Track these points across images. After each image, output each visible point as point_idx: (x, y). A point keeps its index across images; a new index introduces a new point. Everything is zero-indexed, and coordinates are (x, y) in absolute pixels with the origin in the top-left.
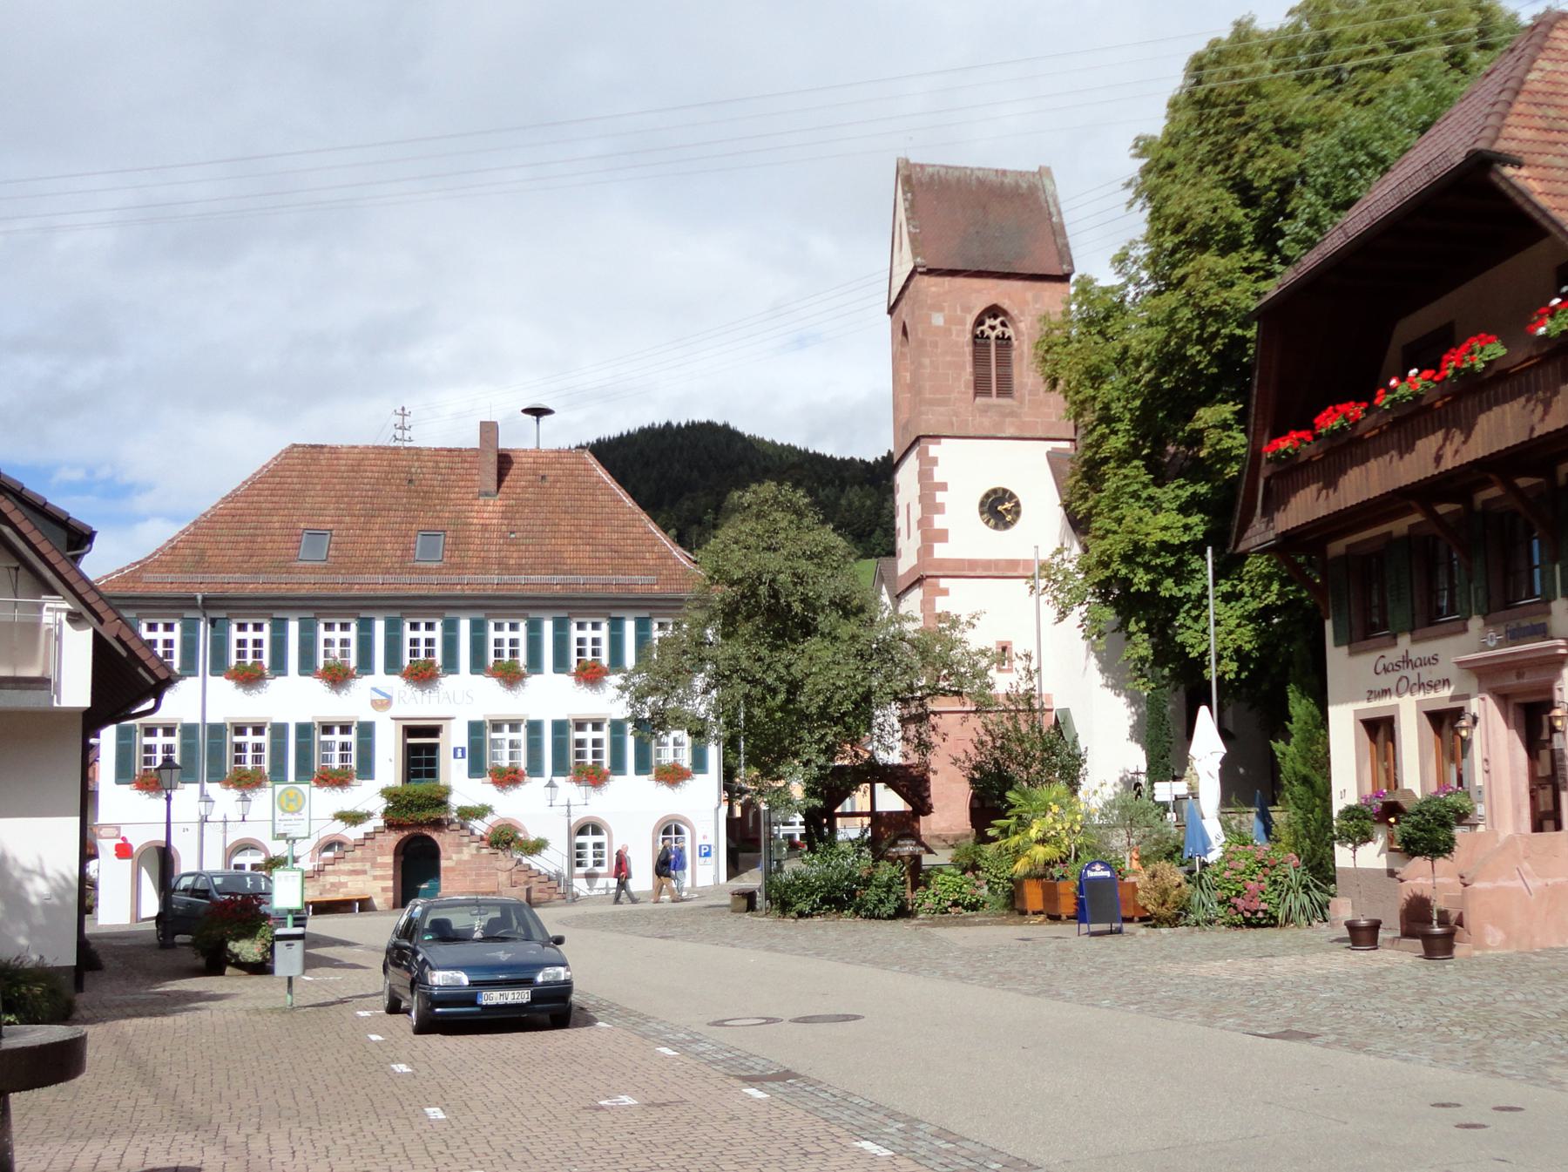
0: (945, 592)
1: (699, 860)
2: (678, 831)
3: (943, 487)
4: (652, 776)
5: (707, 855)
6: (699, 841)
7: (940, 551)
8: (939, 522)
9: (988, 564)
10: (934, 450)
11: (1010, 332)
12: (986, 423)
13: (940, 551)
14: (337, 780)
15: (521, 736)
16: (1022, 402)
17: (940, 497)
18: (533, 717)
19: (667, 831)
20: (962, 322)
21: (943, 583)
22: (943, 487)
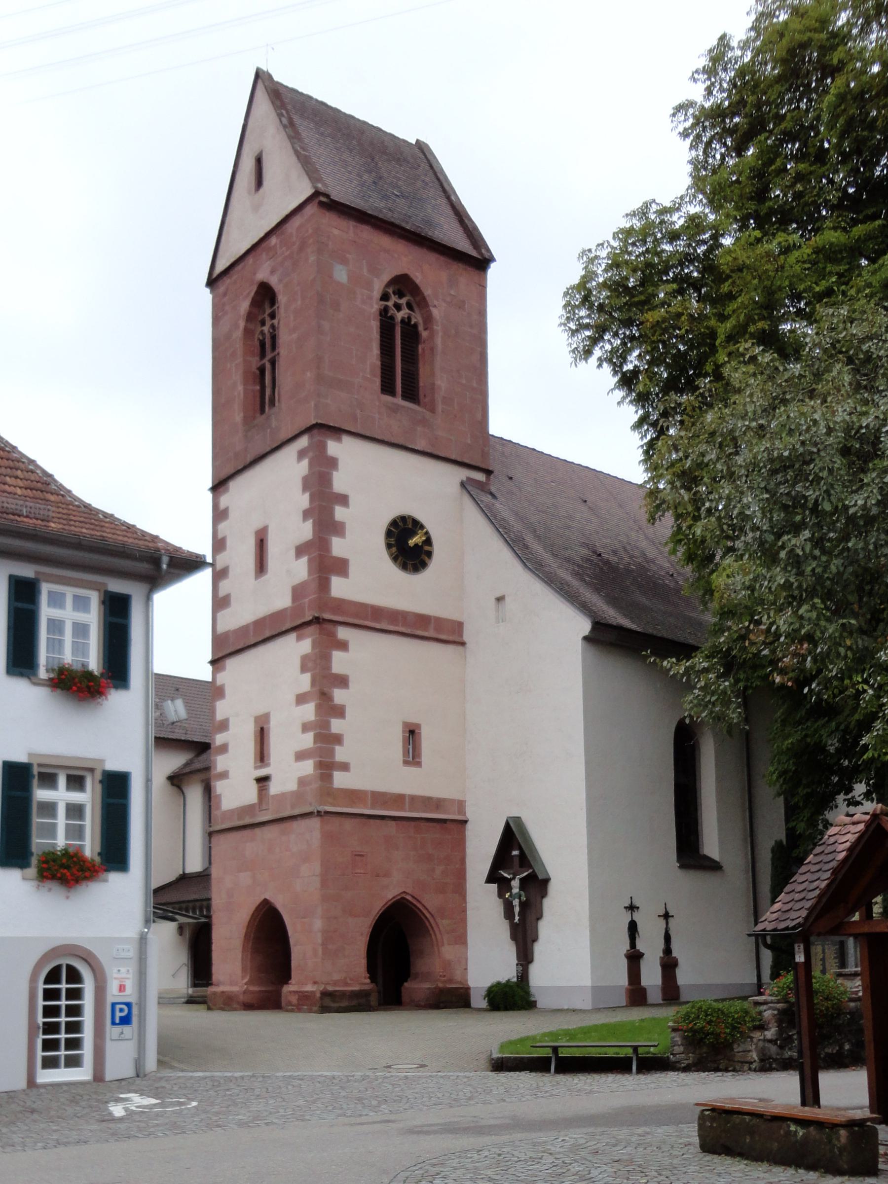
0: (343, 646)
1: (112, 1032)
2: (74, 976)
3: (343, 500)
4: (32, 871)
5: (126, 1020)
6: (113, 994)
7: (339, 587)
8: (338, 547)
9: (395, 616)
10: (333, 448)
11: (417, 318)
12: (395, 427)
13: (339, 587)
14: (66, 872)
15: (88, 797)
16: (433, 411)
17: (340, 513)
18: (113, 765)
19: (53, 976)
20: (369, 285)
21: (343, 633)
22: (343, 500)
